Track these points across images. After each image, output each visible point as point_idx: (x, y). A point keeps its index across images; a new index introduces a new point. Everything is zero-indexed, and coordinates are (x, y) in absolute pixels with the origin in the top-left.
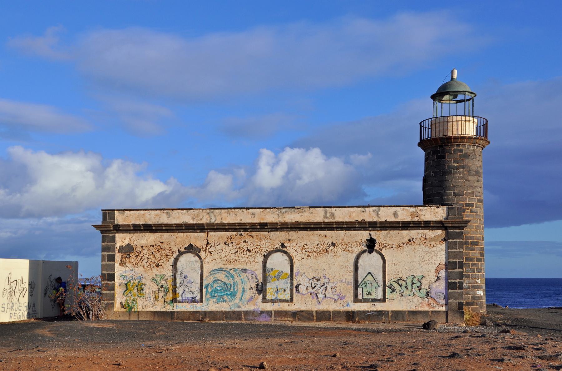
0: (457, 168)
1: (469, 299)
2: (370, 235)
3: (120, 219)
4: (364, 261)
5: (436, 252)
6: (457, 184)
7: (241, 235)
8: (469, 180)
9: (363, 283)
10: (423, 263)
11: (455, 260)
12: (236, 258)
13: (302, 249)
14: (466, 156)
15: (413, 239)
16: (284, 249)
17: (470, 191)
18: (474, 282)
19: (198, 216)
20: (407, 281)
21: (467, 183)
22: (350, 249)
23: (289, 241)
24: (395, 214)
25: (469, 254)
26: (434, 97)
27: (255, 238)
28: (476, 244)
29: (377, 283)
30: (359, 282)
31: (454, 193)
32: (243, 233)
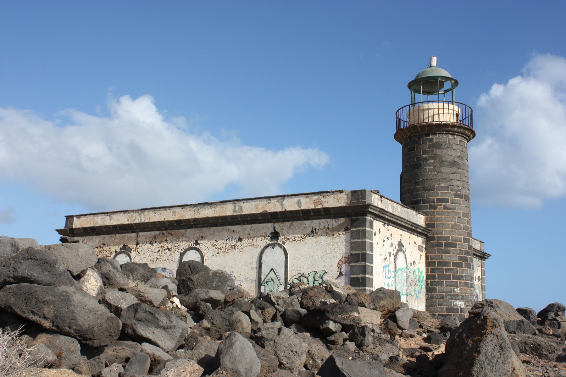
0: (426, 159)
1: (442, 311)
2: (274, 228)
3: (77, 224)
4: (267, 256)
5: (339, 244)
6: (426, 178)
7: (163, 234)
8: (441, 173)
9: (266, 280)
10: (325, 257)
11: (357, 252)
12: (159, 257)
13: (213, 246)
14: (438, 146)
15: (315, 229)
16: (198, 246)
17: (443, 185)
18: (449, 290)
19: (132, 217)
20: (309, 278)
21: (439, 176)
22: (255, 244)
23: (202, 237)
24: (299, 203)
25: (442, 258)
26: (410, 85)
27: (174, 236)
28: (454, 246)
29: (279, 280)
30: (262, 280)
31: (423, 188)
32: (165, 232)
